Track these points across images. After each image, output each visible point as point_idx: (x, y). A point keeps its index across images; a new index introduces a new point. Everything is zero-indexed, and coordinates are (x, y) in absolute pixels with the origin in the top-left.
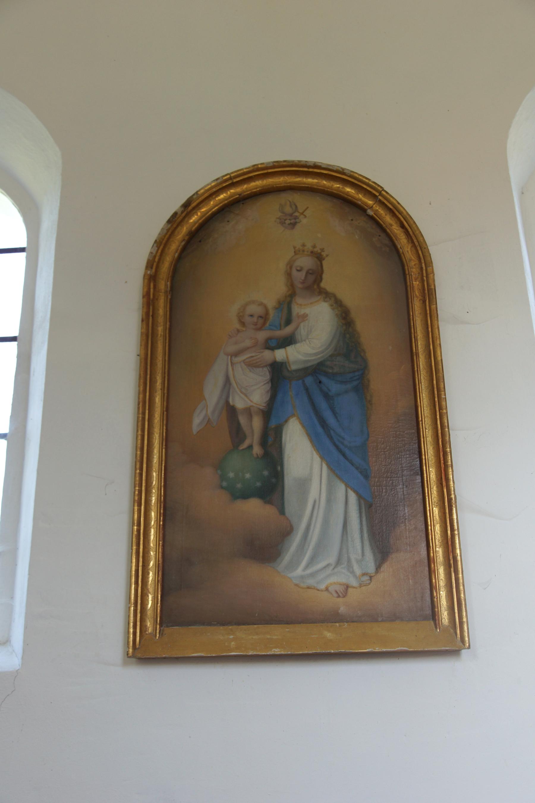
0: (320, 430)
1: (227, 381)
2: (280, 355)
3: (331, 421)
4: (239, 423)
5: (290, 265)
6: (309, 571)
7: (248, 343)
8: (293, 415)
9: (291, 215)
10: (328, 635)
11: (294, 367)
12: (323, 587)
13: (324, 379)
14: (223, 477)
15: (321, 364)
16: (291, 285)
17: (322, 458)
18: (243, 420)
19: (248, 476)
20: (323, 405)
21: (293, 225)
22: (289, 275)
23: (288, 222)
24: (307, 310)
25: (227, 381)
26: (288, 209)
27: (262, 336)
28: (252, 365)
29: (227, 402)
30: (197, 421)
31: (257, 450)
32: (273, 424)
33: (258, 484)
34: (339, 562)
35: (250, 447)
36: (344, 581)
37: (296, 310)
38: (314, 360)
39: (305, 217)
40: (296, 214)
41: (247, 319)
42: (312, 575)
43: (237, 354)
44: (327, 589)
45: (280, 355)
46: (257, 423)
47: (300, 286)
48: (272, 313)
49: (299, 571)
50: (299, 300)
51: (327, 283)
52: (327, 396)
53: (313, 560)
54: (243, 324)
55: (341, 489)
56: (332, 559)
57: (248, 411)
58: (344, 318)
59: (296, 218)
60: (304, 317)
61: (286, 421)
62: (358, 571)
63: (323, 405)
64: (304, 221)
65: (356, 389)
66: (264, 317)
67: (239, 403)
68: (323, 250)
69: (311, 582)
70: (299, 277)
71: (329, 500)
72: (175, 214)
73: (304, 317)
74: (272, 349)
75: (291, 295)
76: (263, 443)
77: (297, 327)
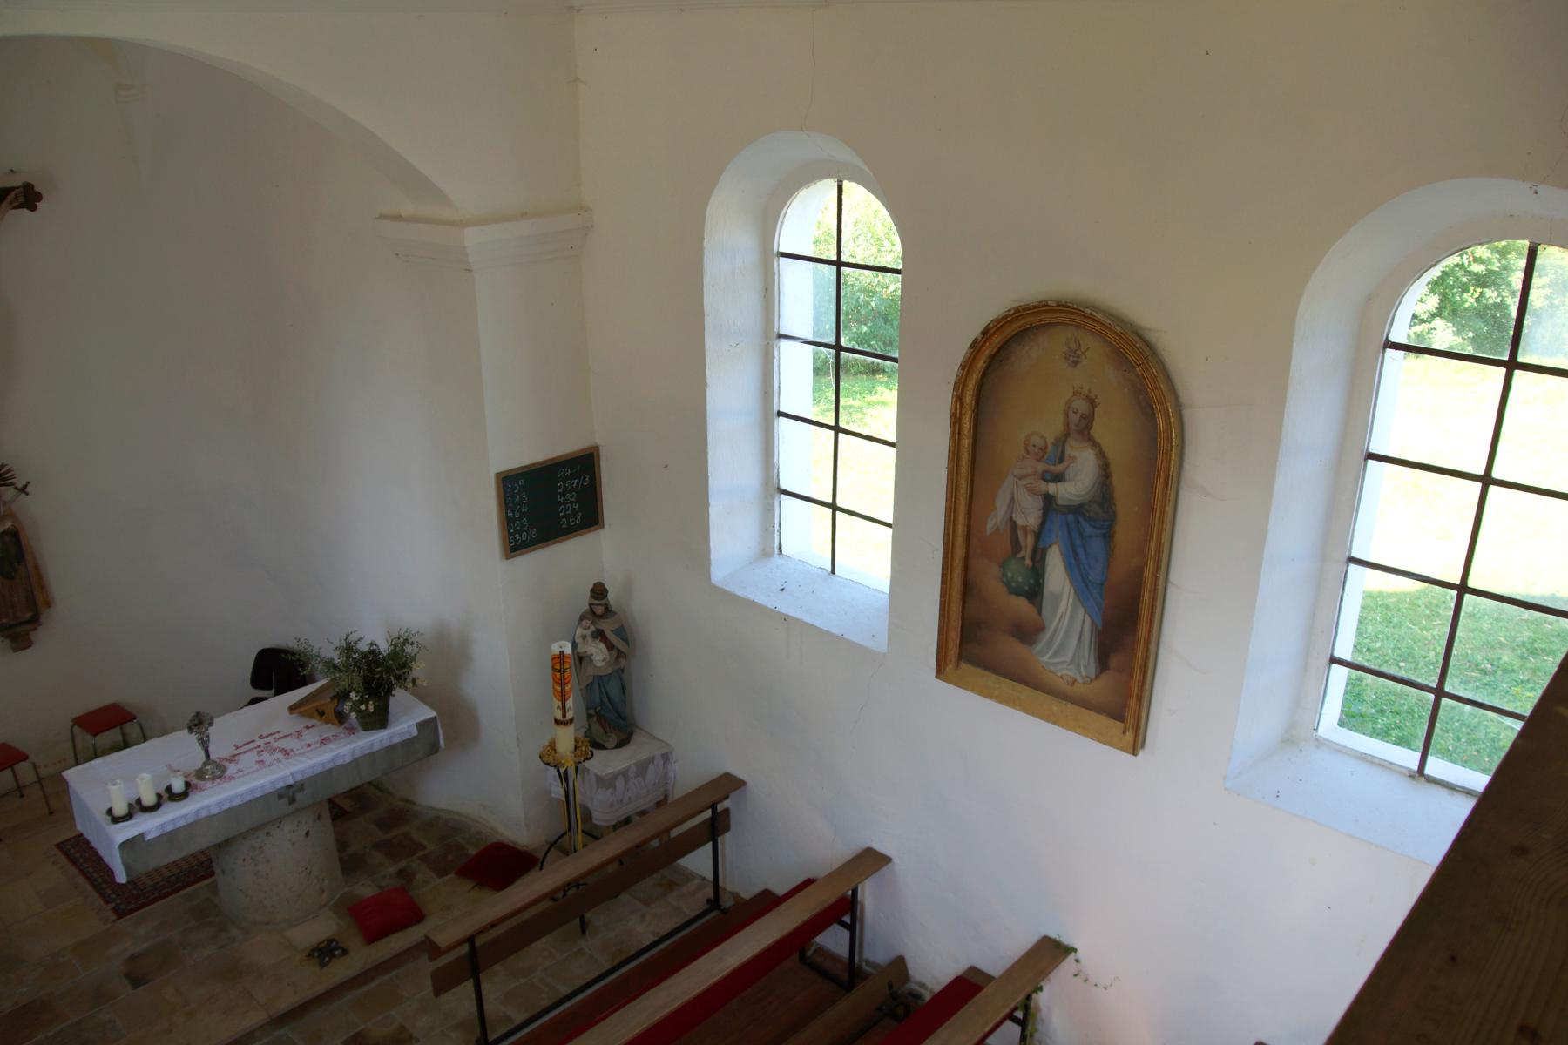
0: (1073, 561)
1: (1012, 500)
2: (1052, 488)
3: (1082, 557)
4: (1017, 538)
5: (1069, 404)
6: (1051, 661)
7: (1030, 471)
8: (1055, 543)
9: (1075, 352)
10: (1055, 708)
11: (1061, 502)
12: (1059, 674)
13: (1081, 520)
14: (1004, 575)
15: (1081, 506)
16: (1067, 425)
17: (1072, 583)
18: (1020, 534)
19: (1020, 579)
20: (1078, 542)
21: (1076, 363)
22: (1067, 415)
23: (1071, 358)
24: (1076, 454)
25: (1012, 500)
26: (1073, 346)
27: (1041, 467)
28: (1032, 491)
29: (1011, 517)
30: (990, 525)
31: (1028, 562)
32: (1041, 545)
33: (1027, 588)
34: (1072, 662)
35: (1024, 558)
36: (1073, 675)
37: (1068, 451)
38: (1077, 501)
39: (1086, 358)
40: (1079, 352)
41: (1031, 448)
42: (1054, 664)
43: (1021, 478)
44: (1061, 677)
45: (1052, 488)
46: (1030, 541)
47: (1074, 428)
48: (1050, 448)
49: (1046, 658)
50: (1071, 442)
51: (1097, 431)
52: (1081, 534)
53: (1055, 655)
54: (1028, 452)
55: (1081, 612)
56: (1068, 658)
57: (1025, 528)
58: (1105, 470)
59: (1078, 356)
60: (1074, 459)
61: (1050, 546)
62: (1083, 673)
63: (1078, 542)
64: (1085, 362)
65: (1104, 536)
66: (1044, 450)
67: (1020, 521)
68: (1096, 397)
69: (1052, 668)
70: (1075, 418)
71: (1072, 617)
72: (976, 340)
73: (1074, 459)
74: (1047, 481)
75: (1067, 435)
76: (1033, 558)
77: (1068, 467)
